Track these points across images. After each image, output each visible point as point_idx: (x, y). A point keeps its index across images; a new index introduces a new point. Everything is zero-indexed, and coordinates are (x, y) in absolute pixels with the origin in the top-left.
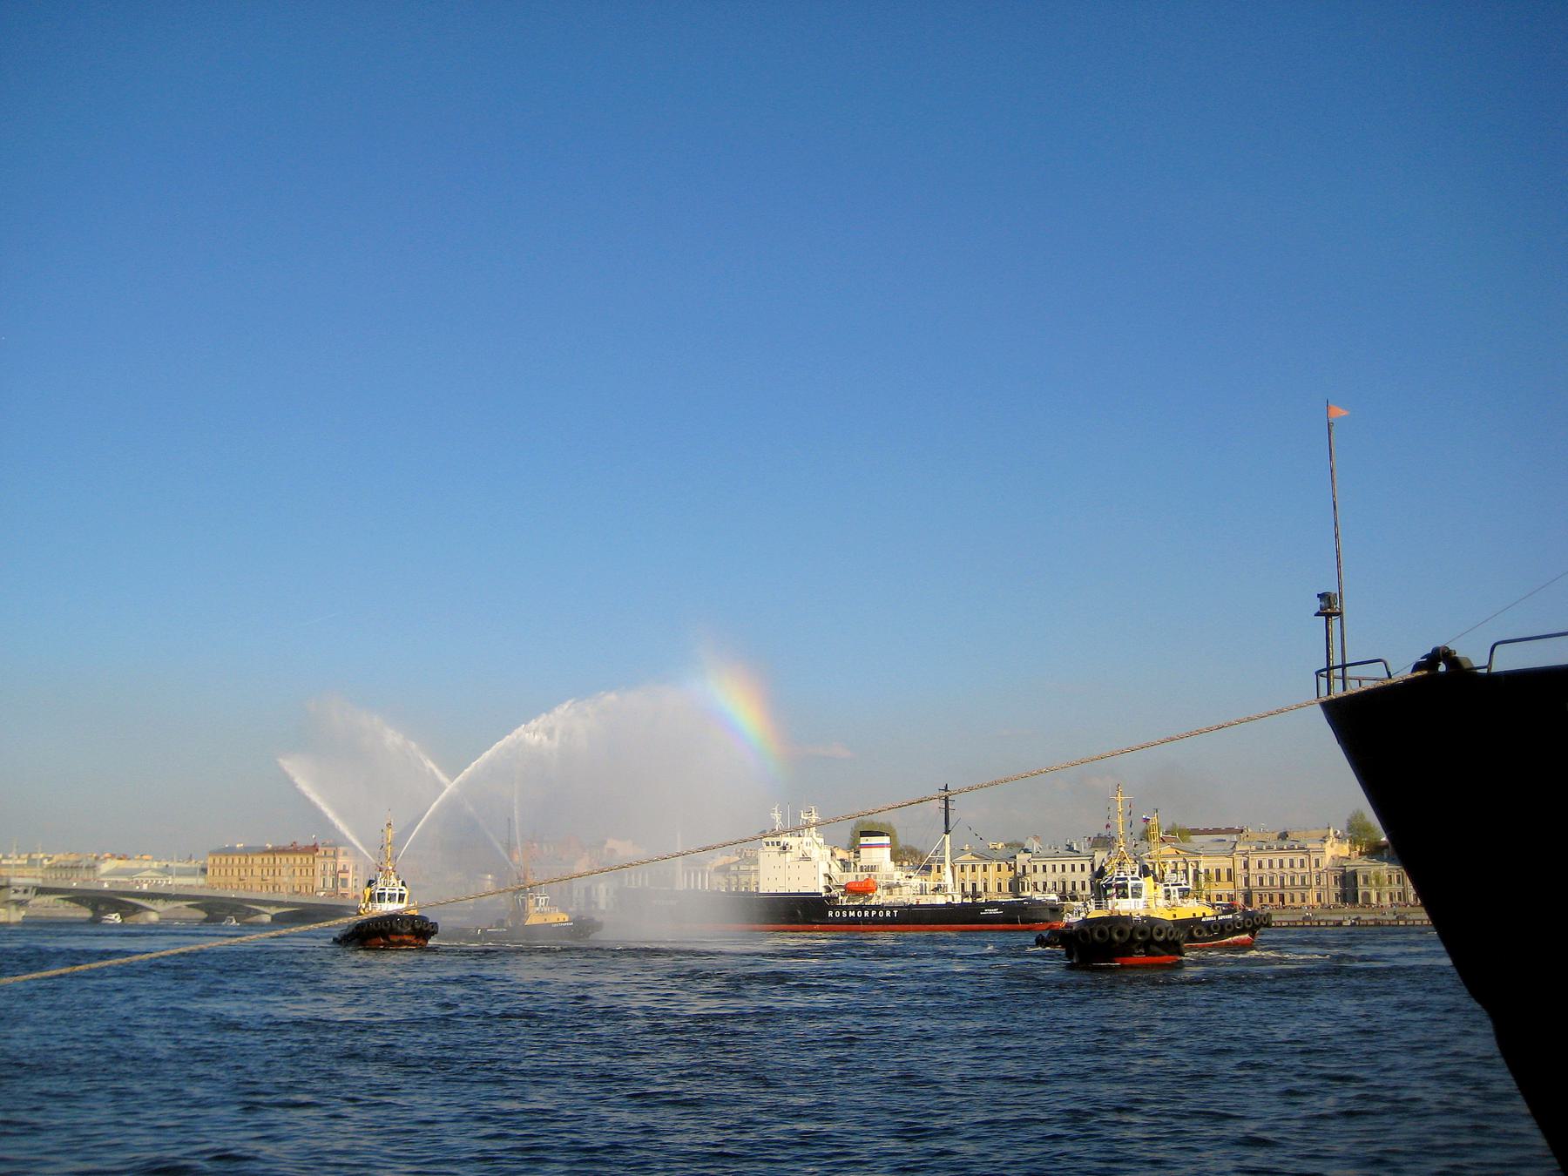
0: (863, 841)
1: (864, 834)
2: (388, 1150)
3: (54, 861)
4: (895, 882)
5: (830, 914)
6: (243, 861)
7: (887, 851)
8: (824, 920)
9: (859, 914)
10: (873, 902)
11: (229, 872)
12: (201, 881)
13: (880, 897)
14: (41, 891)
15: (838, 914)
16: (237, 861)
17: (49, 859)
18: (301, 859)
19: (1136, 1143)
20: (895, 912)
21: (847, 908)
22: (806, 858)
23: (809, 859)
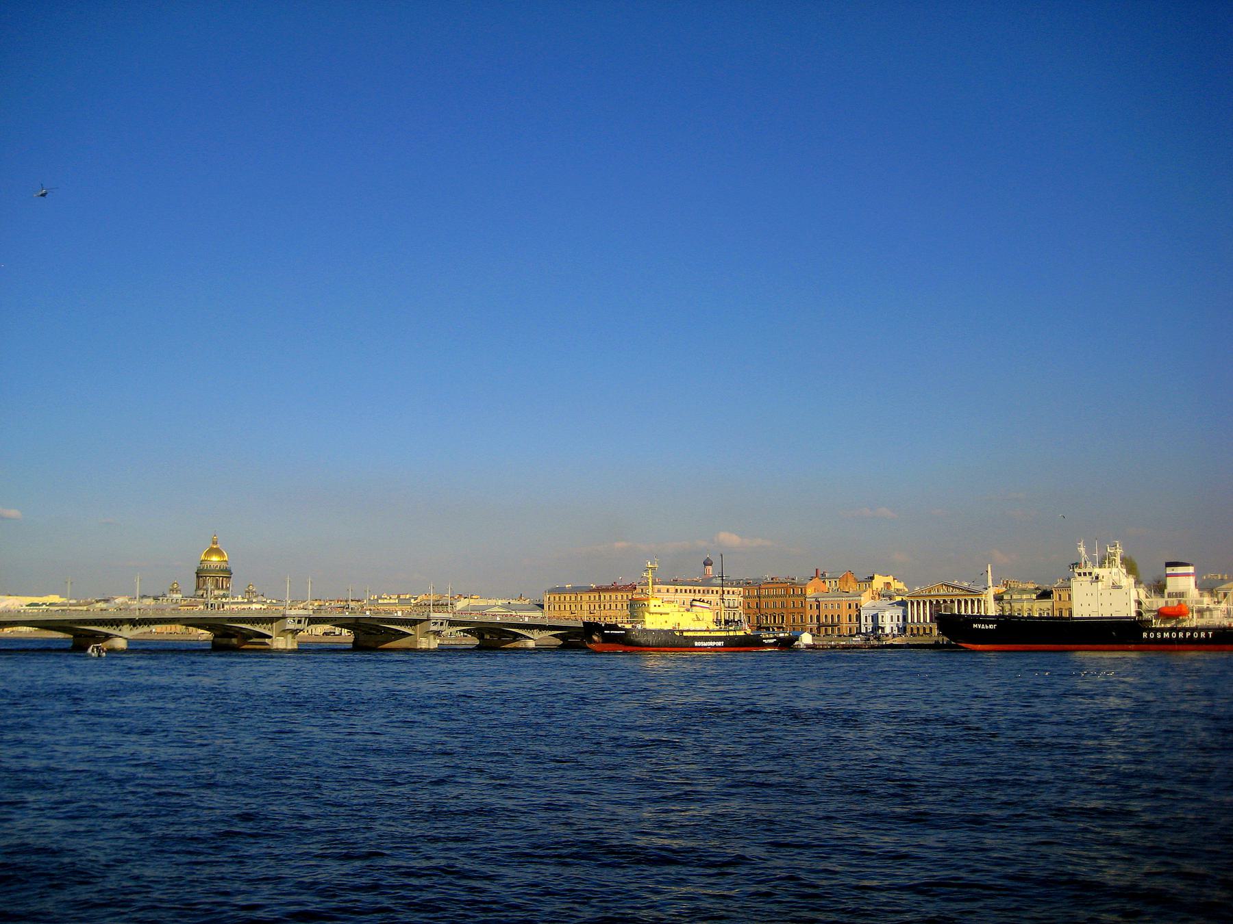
0: (1169, 570)
1: (1169, 565)
2: (337, 825)
3: (418, 600)
4: (1205, 606)
5: (1145, 635)
6: (573, 599)
7: (1192, 580)
8: (1138, 640)
9: (1174, 635)
10: (1186, 624)
11: (562, 608)
12: (538, 614)
13: (1193, 621)
14: (313, 621)
15: (1152, 635)
16: (568, 599)
17: (416, 599)
18: (622, 596)
19: (552, 844)
20: (1210, 633)
21: (1162, 630)
22: (1116, 586)
23: (1120, 587)
